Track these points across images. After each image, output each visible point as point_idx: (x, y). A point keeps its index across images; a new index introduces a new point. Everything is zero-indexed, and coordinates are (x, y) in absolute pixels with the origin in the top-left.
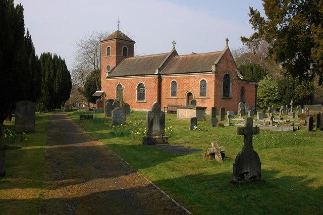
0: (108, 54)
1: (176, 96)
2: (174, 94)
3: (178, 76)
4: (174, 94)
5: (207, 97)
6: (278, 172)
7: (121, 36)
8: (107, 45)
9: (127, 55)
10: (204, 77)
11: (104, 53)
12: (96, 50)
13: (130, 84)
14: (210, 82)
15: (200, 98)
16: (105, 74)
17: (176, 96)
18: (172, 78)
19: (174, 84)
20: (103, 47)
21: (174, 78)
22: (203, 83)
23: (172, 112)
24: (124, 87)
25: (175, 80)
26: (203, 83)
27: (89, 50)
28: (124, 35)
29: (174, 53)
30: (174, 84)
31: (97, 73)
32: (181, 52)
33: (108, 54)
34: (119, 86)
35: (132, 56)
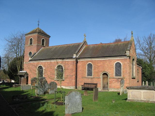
0: (31, 43)
1: (91, 75)
2: (90, 74)
3: (93, 60)
4: (90, 74)
5: (92, 77)
6: (25, 92)
7: (40, 31)
8: (30, 37)
9: (45, 45)
10: (118, 60)
11: (28, 43)
12: (18, 45)
13: (49, 67)
14: (124, 64)
15: (86, 77)
16: (27, 58)
17: (91, 75)
18: (88, 61)
19: (90, 66)
20: (27, 39)
21: (89, 61)
22: (118, 66)
23: (88, 89)
24: (44, 68)
25: (91, 63)
26: (118, 66)
27: (13, 44)
28: (43, 31)
29: (85, 42)
30: (90, 66)
31: (21, 59)
32: (89, 43)
33: (31, 43)
34: (40, 67)
35: (48, 46)
